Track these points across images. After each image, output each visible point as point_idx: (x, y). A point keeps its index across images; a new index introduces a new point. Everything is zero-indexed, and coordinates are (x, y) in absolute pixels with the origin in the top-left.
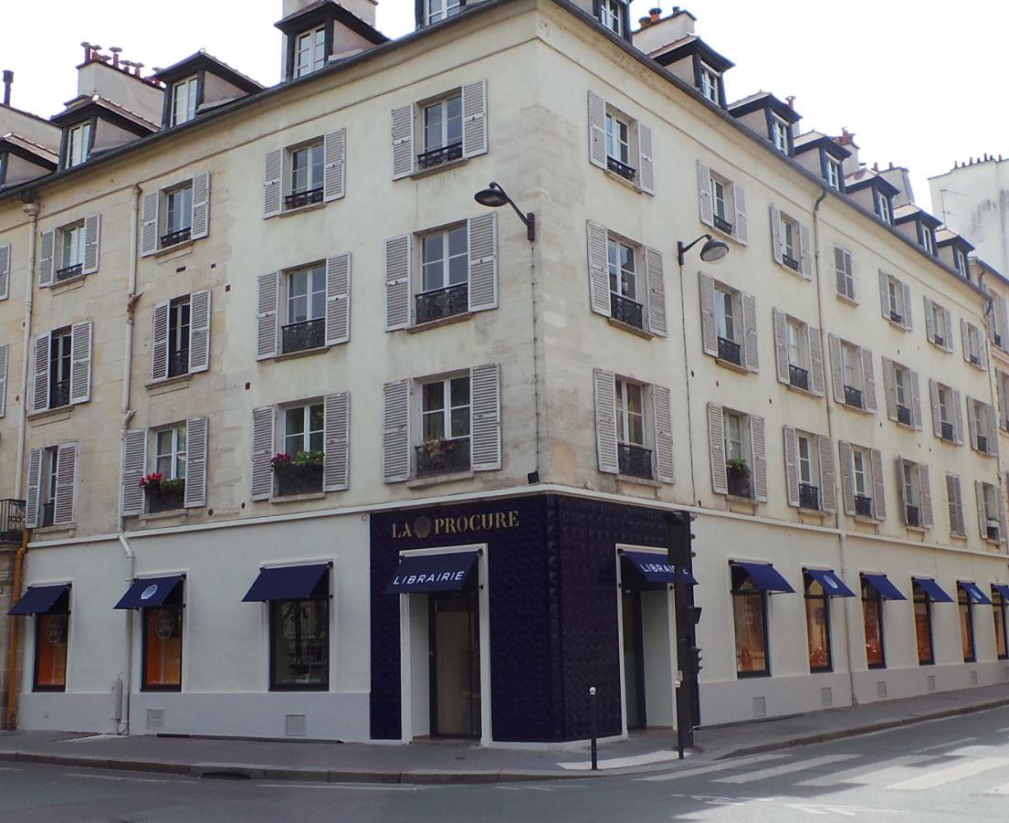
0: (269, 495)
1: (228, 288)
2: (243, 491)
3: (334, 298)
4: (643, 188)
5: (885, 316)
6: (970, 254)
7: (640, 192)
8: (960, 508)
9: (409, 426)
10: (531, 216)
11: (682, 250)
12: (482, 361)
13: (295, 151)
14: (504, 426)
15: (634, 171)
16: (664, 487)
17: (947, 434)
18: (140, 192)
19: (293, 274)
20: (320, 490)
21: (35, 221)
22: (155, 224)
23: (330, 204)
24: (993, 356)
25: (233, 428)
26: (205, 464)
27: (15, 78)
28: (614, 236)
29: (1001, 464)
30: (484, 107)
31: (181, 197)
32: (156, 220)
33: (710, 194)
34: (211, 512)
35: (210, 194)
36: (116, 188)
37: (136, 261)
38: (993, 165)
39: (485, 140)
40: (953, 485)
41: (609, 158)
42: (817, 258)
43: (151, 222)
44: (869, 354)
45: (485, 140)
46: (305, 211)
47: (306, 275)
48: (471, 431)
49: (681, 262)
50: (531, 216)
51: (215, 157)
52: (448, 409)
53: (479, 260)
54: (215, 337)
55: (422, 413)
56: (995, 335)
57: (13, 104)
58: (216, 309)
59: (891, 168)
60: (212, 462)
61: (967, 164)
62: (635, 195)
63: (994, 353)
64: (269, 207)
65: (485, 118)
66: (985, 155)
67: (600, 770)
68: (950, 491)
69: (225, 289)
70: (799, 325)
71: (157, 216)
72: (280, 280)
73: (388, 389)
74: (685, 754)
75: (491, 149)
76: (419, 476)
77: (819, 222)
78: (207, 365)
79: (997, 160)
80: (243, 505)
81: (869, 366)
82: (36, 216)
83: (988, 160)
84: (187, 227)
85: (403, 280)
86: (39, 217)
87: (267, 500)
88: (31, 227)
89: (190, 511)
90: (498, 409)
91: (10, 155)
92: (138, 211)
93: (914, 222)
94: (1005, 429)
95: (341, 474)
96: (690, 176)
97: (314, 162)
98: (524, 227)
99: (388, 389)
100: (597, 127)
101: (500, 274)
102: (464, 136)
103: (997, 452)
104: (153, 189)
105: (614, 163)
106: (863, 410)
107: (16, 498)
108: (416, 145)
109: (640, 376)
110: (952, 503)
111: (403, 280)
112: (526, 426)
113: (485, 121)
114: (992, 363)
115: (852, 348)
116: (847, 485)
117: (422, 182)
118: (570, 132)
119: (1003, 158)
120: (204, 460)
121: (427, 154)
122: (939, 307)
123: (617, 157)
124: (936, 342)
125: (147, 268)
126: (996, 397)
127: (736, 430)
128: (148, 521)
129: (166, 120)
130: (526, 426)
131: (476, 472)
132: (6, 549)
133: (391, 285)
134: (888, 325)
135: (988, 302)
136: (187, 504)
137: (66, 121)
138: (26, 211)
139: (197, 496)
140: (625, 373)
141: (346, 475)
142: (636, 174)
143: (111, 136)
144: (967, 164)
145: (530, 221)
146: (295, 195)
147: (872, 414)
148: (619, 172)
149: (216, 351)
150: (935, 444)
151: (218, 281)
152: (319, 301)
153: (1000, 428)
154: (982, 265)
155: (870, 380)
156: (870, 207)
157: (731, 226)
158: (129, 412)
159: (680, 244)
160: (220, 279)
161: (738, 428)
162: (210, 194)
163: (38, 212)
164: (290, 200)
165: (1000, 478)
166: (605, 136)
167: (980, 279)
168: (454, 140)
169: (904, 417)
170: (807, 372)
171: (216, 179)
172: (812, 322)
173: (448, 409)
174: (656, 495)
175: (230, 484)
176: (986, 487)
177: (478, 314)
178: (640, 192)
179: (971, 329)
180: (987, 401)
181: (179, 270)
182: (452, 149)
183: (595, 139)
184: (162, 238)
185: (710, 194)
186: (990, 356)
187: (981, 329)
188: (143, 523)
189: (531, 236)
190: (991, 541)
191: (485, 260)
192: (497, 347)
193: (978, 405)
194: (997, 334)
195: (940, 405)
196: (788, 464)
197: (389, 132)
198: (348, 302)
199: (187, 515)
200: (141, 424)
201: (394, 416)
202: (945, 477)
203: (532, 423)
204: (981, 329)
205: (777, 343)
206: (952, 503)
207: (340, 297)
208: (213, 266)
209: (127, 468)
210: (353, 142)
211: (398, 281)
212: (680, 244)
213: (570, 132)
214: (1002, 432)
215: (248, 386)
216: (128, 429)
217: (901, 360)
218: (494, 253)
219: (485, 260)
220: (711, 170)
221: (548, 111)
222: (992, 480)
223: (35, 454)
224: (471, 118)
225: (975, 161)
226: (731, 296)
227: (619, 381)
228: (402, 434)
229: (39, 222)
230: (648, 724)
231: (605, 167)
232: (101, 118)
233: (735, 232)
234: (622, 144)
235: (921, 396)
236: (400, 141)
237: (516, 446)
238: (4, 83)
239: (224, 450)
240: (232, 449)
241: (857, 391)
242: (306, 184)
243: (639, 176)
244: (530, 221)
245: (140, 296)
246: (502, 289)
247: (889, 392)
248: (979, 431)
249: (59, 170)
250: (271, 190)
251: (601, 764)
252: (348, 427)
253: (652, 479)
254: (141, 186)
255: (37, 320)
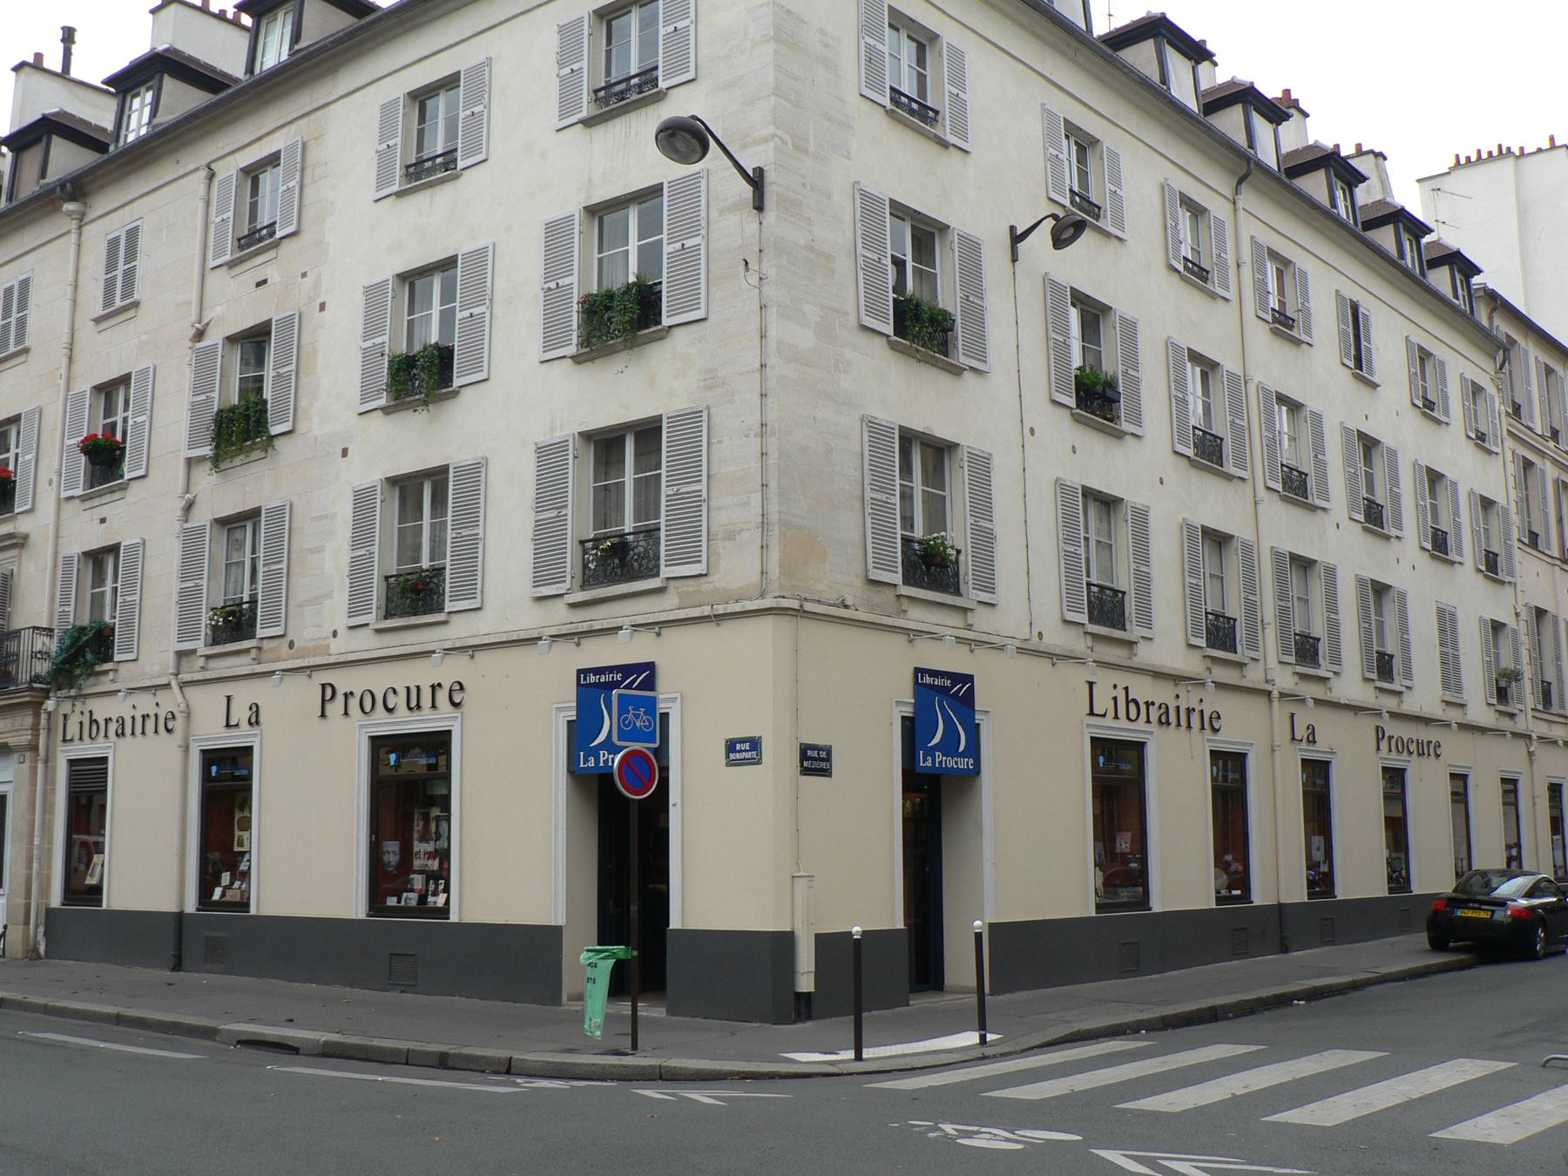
0: (370, 618)
1: (322, 307)
2: (336, 612)
3: (466, 314)
4: (951, 139)
5: (1347, 362)
6: (1476, 280)
7: (944, 145)
8: (1456, 657)
9: (570, 507)
10: (760, 171)
11: (1017, 238)
12: (680, 404)
13: (421, 98)
14: (712, 504)
15: (937, 112)
16: (981, 610)
17: (1439, 545)
18: (211, 176)
19: (412, 279)
20: (440, 609)
21: (80, 227)
22: (226, 216)
23: (468, 171)
24: (1508, 430)
25: (321, 518)
26: (285, 571)
27: (77, 37)
28: (899, 211)
29: (1519, 594)
30: (692, 10)
31: (266, 180)
32: (231, 214)
33: (1064, 156)
34: (291, 644)
35: (303, 169)
36: (182, 172)
37: (203, 276)
38: (1511, 161)
39: (692, 60)
40: (1447, 621)
41: (892, 88)
42: (1238, 266)
43: (225, 216)
44: (1317, 419)
45: (692, 60)
46: (431, 185)
47: (431, 284)
48: (663, 513)
49: (1014, 259)
50: (760, 171)
51: (313, 116)
52: (629, 476)
53: (680, 244)
54: (303, 381)
55: (592, 485)
56: (1513, 402)
57: (75, 73)
58: (306, 339)
59: (1360, 152)
60: (295, 568)
61: (1473, 159)
62: (933, 149)
63: (1510, 429)
64: (382, 181)
65: (692, 28)
66: (1500, 147)
67: (867, 1060)
68: (1442, 631)
69: (318, 307)
70: (1208, 367)
71: (232, 209)
72: (393, 290)
73: (543, 452)
74: (990, 1037)
75: (701, 72)
76: (585, 585)
77: (1241, 213)
78: (291, 422)
79: (1517, 153)
80: (335, 634)
81: (1318, 436)
82: (81, 220)
83: (1504, 153)
84: (272, 221)
85: (566, 281)
86: (86, 220)
87: (367, 625)
88: (73, 237)
89: (265, 642)
90: (704, 478)
91: (54, 137)
92: (208, 203)
93: (1392, 225)
94: (1526, 541)
95: (470, 584)
96: (1034, 128)
97: (447, 113)
98: (747, 190)
99: (543, 452)
100: (872, 42)
101: (711, 267)
102: (660, 58)
103: (1511, 574)
104: (228, 170)
105: (903, 99)
106: (1209, 286)
107: (44, 626)
108: (589, 74)
109: (943, 431)
110: (1445, 650)
111: (566, 281)
112: (745, 504)
113: (692, 32)
114: (1509, 443)
115: (1294, 407)
116: (1284, 614)
117: (599, 131)
118: (827, 46)
119: (1526, 151)
120: (284, 566)
121: (608, 86)
122: (1429, 355)
123: (908, 87)
124: (1425, 406)
125: (217, 280)
126: (1513, 494)
127: (1106, 525)
128: (208, 657)
129: (250, 68)
130: (745, 504)
131: (668, 579)
132: (28, 699)
133: (550, 289)
134: (1351, 377)
135: (1501, 352)
136: (260, 633)
137: (126, 83)
138: (69, 214)
139: (272, 621)
140: (917, 425)
141: (479, 586)
142: (939, 118)
143: (181, 99)
144: (1473, 159)
145: (756, 181)
146: (420, 162)
147: (1324, 509)
148: (912, 112)
149: (303, 403)
150: (1423, 560)
151: (310, 297)
152: (447, 318)
153: (1519, 540)
154: (1492, 297)
155: (1320, 456)
156: (1322, 197)
157: (1099, 208)
158: (188, 496)
159: (1012, 228)
160: (312, 294)
161: (1109, 523)
162: (303, 169)
163: (83, 215)
164: (411, 170)
165: (1517, 615)
166: (887, 55)
167: (1491, 319)
168: (648, 64)
169: (1374, 517)
170: (1222, 439)
171: (311, 146)
172: (1229, 363)
173: (629, 476)
174: (966, 620)
175: (317, 600)
176: (1497, 627)
177: (675, 329)
178: (944, 145)
179: (1477, 390)
180: (1500, 498)
181: (259, 284)
182: (644, 77)
183: (872, 59)
184: (239, 240)
185: (1064, 156)
186: (1505, 433)
187: (1490, 389)
188: (201, 662)
189: (759, 206)
190: (1502, 708)
191: (688, 243)
192: (705, 380)
193: (1487, 504)
194: (1516, 400)
195: (1428, 500)
196: (1188, 579)
197: (553, 59)
198: (487, 319)
199: (259, 649)
200: (203, 516)
201: (548, 492)
202: (1434, 610)
203: (756, 498)
204: (1490, 389)
205: (1174, 392)
206: (1445, 650)
207: (475, 311)
208: (304, 275)
209: (183, 579)
210: (500, 77)
211: (561, 282)
212: (1012, 228)
213: (827, 46)
214: (1521, 546)
215: (345, 453)
216: (186, 521)
217: (1370, 429)
218: (703, 232)
219: (688, 243)
220: (1065, 119)
221: (789, 12)
222: (1505, 616)
223: (68, 560)
224: (671, 28)
225: (1484, 156)
226: (1093, 314)
227: (908, 438)
228: (560, 519)
229: (86, 230)
230: (947, 981)
231: (886, 101)
232: (170, 75)
233: (1105, 217)
234: (919, 72)
235: (1402, 483)
236: (567, 70)
237: (730, 536)
238: (62, 45)
239: (311, 551)
240: (321, 550)
241: (1301, 473)
242: (435, 146)
243: (944, 119)
244: (756, 181)
245: (207, 324)
246: (713, 289)
247: (1352, 479)
248: (1488, 544)
249: (112, 148)
250: (384, 158)
251: (867, 1053)
252: (482, 511)
253: (960, 595)
254: (213, 166)
255: (78, 368)
